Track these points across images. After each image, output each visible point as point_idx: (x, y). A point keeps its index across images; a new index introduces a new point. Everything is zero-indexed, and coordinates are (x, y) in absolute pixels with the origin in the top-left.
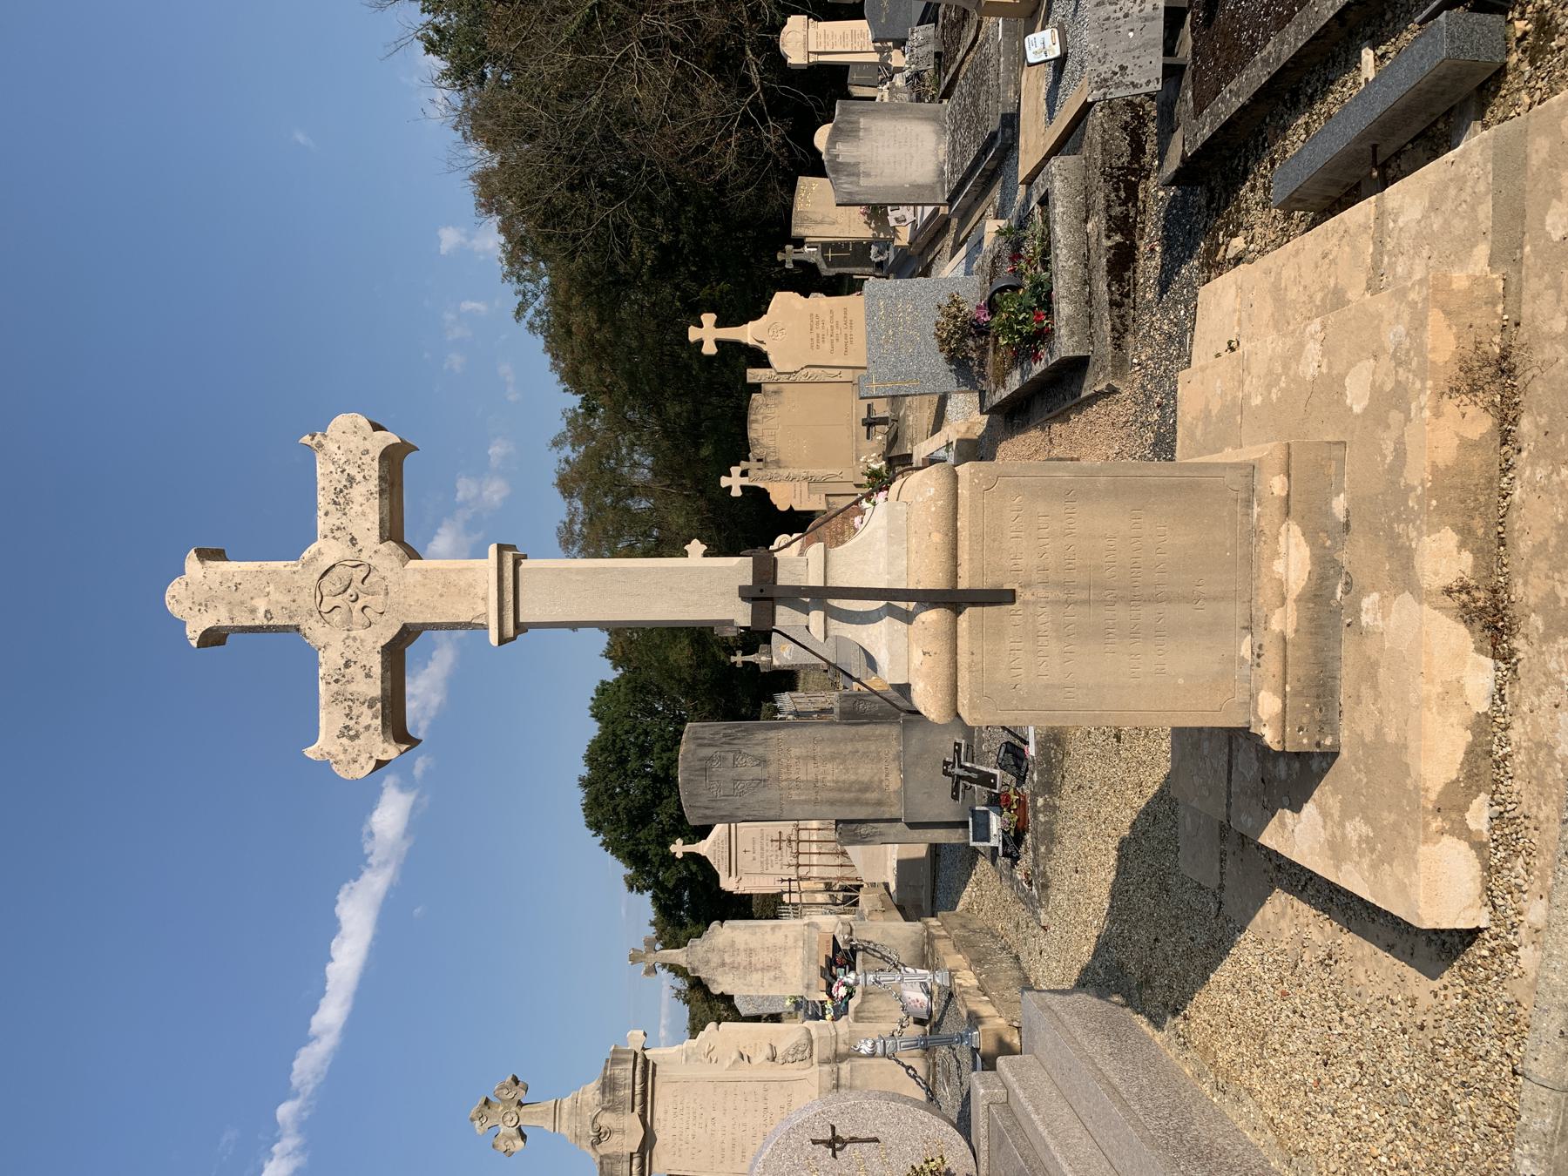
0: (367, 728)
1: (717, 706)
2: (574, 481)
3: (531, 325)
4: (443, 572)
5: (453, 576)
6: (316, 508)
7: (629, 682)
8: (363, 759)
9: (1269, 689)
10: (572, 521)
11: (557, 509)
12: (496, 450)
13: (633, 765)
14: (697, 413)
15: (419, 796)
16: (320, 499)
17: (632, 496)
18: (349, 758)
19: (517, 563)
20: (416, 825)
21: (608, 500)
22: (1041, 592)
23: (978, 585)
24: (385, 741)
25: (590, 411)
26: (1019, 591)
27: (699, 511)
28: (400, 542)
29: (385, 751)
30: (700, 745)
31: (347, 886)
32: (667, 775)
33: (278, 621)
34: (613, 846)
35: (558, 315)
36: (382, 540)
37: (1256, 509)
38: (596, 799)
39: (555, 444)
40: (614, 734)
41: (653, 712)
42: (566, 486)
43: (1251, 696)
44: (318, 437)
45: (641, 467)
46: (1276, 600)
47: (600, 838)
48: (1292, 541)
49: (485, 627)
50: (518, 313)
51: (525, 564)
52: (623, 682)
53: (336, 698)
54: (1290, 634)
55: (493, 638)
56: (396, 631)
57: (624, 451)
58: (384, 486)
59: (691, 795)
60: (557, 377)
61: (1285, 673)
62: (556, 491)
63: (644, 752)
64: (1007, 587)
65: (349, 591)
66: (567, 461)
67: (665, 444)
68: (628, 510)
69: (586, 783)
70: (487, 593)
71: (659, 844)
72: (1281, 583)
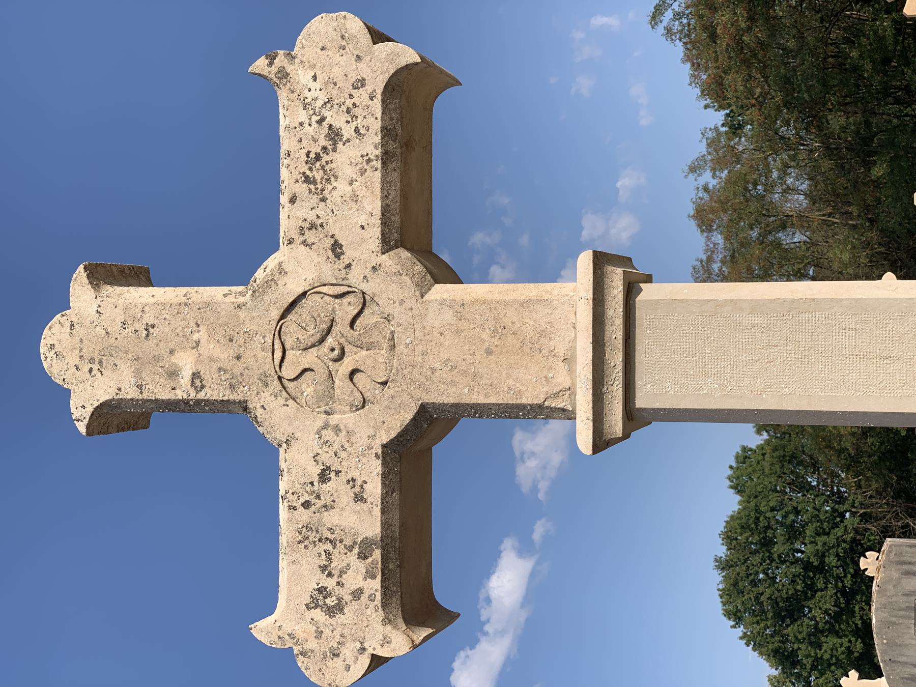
0: (357, 594)
1: (887, 484)
2: (713, 211)
3: (669, 31)
4: (492, 306)
5: (511, 316)
6: (278, 191)
7: (775, 449)
8: (349, 651)
10: (710, 259)
11: (695, 243)
12: (626, 182)
13: (779, 548)
14: (868, 124)
15: (538, 563)
16: (284, 173)
17: (783, 227)
18: (325, 648)
19: (631, 291)
20: (535, 593)
21: (754, 234)
24: (386, 621)
25: (735, 129)
27: (868, 244)
28: (423, 251)
29: (386, 641)
30: (908, 573)
31: (462, 654)
32: (822, 562)
33: (213, 393)
34: (756, 641)
35: (701, 17)
36: (387, 246)
38: (735, 584)
39: (693, 169)
40: (757, 510)
41: (805, 487)
42: (703, 218)
44: (281, 59)
45: (794, 192)
47: (740, 631)
49: (569, 415)
50: (654, 17)
51: (648, 292)
52: (768, 449)
53: (308, 535)
55: (584, 440)
56: (407, 416)
57: (775, 174)
58: (392, 146)
59: (892, 644)
60: (698, 91)
62: (693, 223)
63: (794, 533)
65: (330, 340)
66: (706, 189)
67: (826, 164)
68: (778, 244)
69: (724, 565)
70: (573, 349)
71: (811, 644)
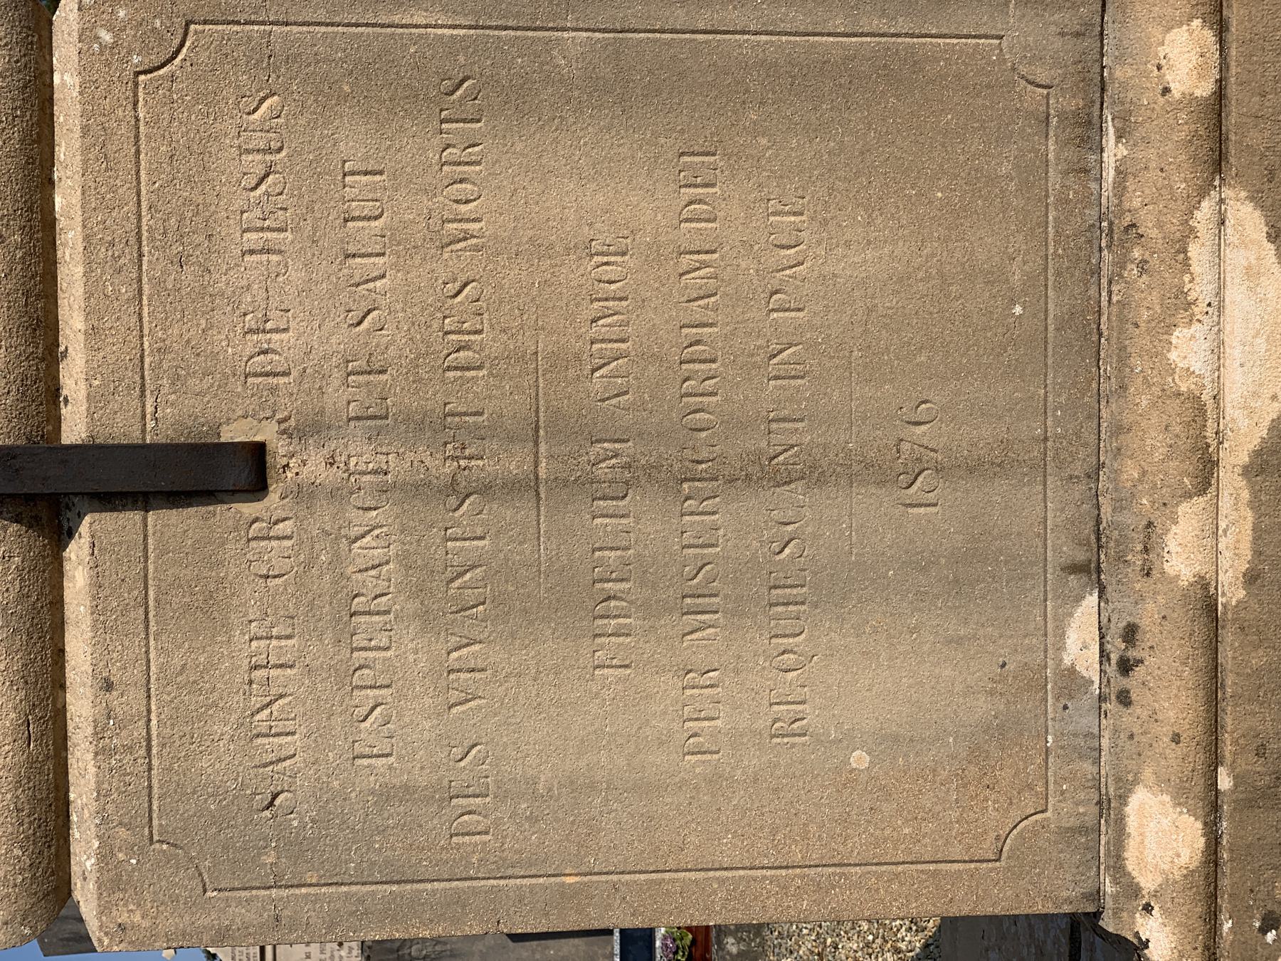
9: (1162, 782)
22: (361, 454)
23: (124, 427)
26: (279, 448)
37: (1113, 151)
43: (1102, 804)
46: (1181, 471)
48: (1236, 259)
54: (1231, 592)
61: (1214, 727)
64: (234, 433)
72: (1198, 415)
